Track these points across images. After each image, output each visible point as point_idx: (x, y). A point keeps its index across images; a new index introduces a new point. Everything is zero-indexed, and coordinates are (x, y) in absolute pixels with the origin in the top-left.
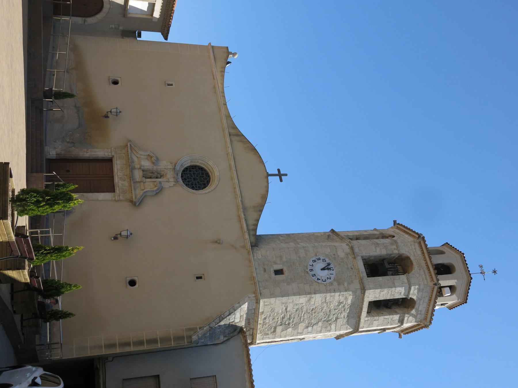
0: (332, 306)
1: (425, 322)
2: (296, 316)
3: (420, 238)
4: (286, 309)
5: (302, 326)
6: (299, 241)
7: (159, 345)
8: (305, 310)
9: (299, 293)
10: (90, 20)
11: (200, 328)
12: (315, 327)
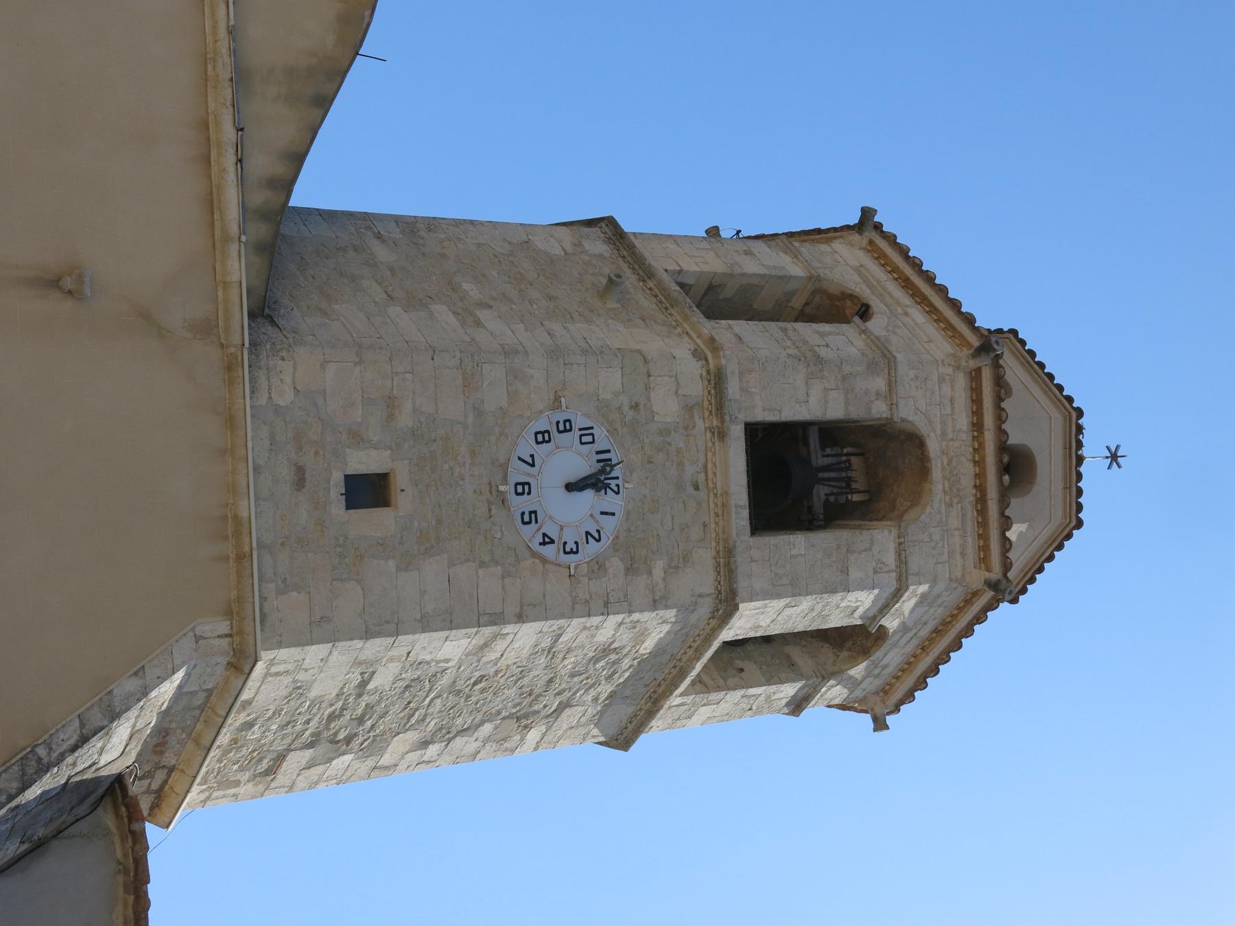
4: (363, 684)
5: (399, 744)
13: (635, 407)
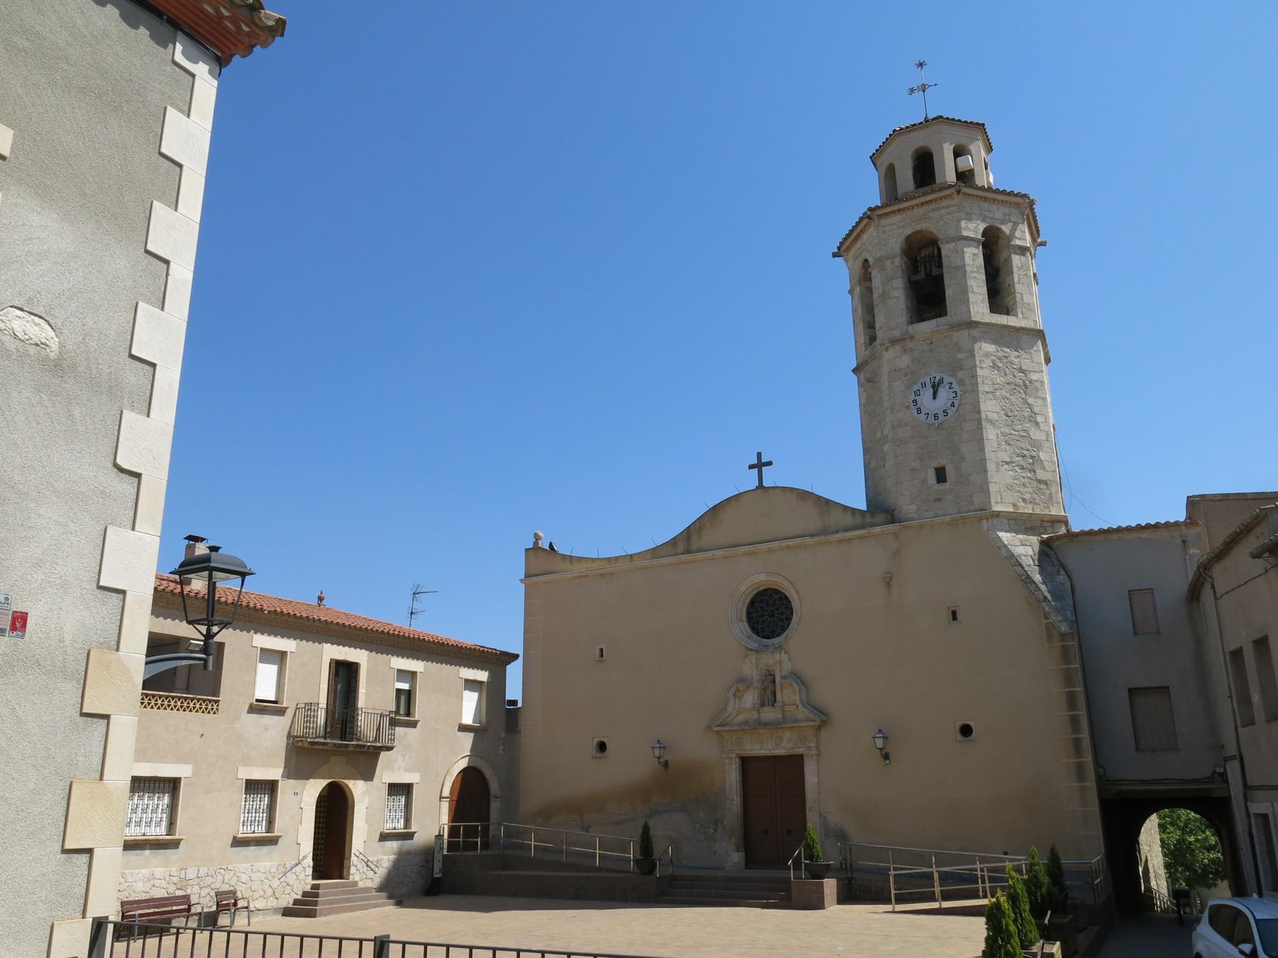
0: (1000, 380)
1: (1023, 206)
2: (1019, 444)
3: (870, 216)
4: (1007, 463)
5: (1035, 434)
6: (879, 435)
7: (1079, 689)
8: (1007, 430)
9: (980, 440)
10: (494, 787)
11: (1046, 618)
12: (1036, 410)
13: (906, 374)
